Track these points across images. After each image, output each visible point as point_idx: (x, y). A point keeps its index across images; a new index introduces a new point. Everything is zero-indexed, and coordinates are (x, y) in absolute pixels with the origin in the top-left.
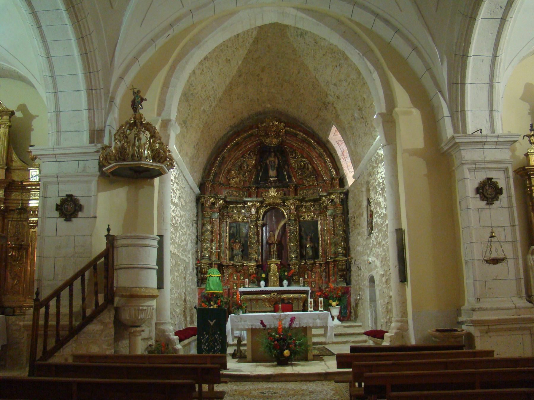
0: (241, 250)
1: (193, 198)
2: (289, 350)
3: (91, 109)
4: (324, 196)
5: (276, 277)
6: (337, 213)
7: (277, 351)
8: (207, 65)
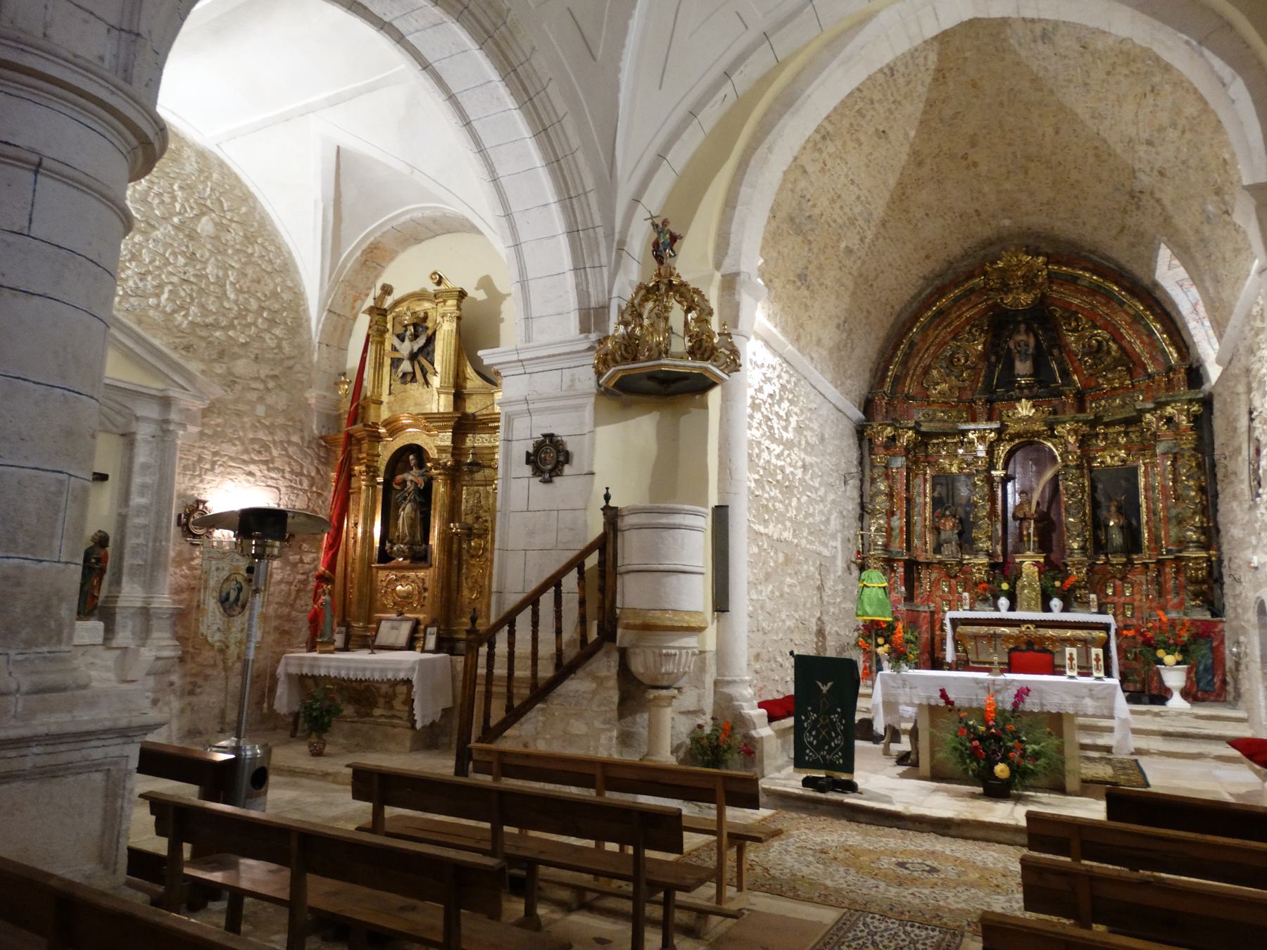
0: (956, 531)
1: (848, 429)
2: (1009, 765)
3: (578, 268)
4: (1149, 411)
5: (1034, 590)
6: (1183, 449)
7: (978, 764)
8: (831, 149)
